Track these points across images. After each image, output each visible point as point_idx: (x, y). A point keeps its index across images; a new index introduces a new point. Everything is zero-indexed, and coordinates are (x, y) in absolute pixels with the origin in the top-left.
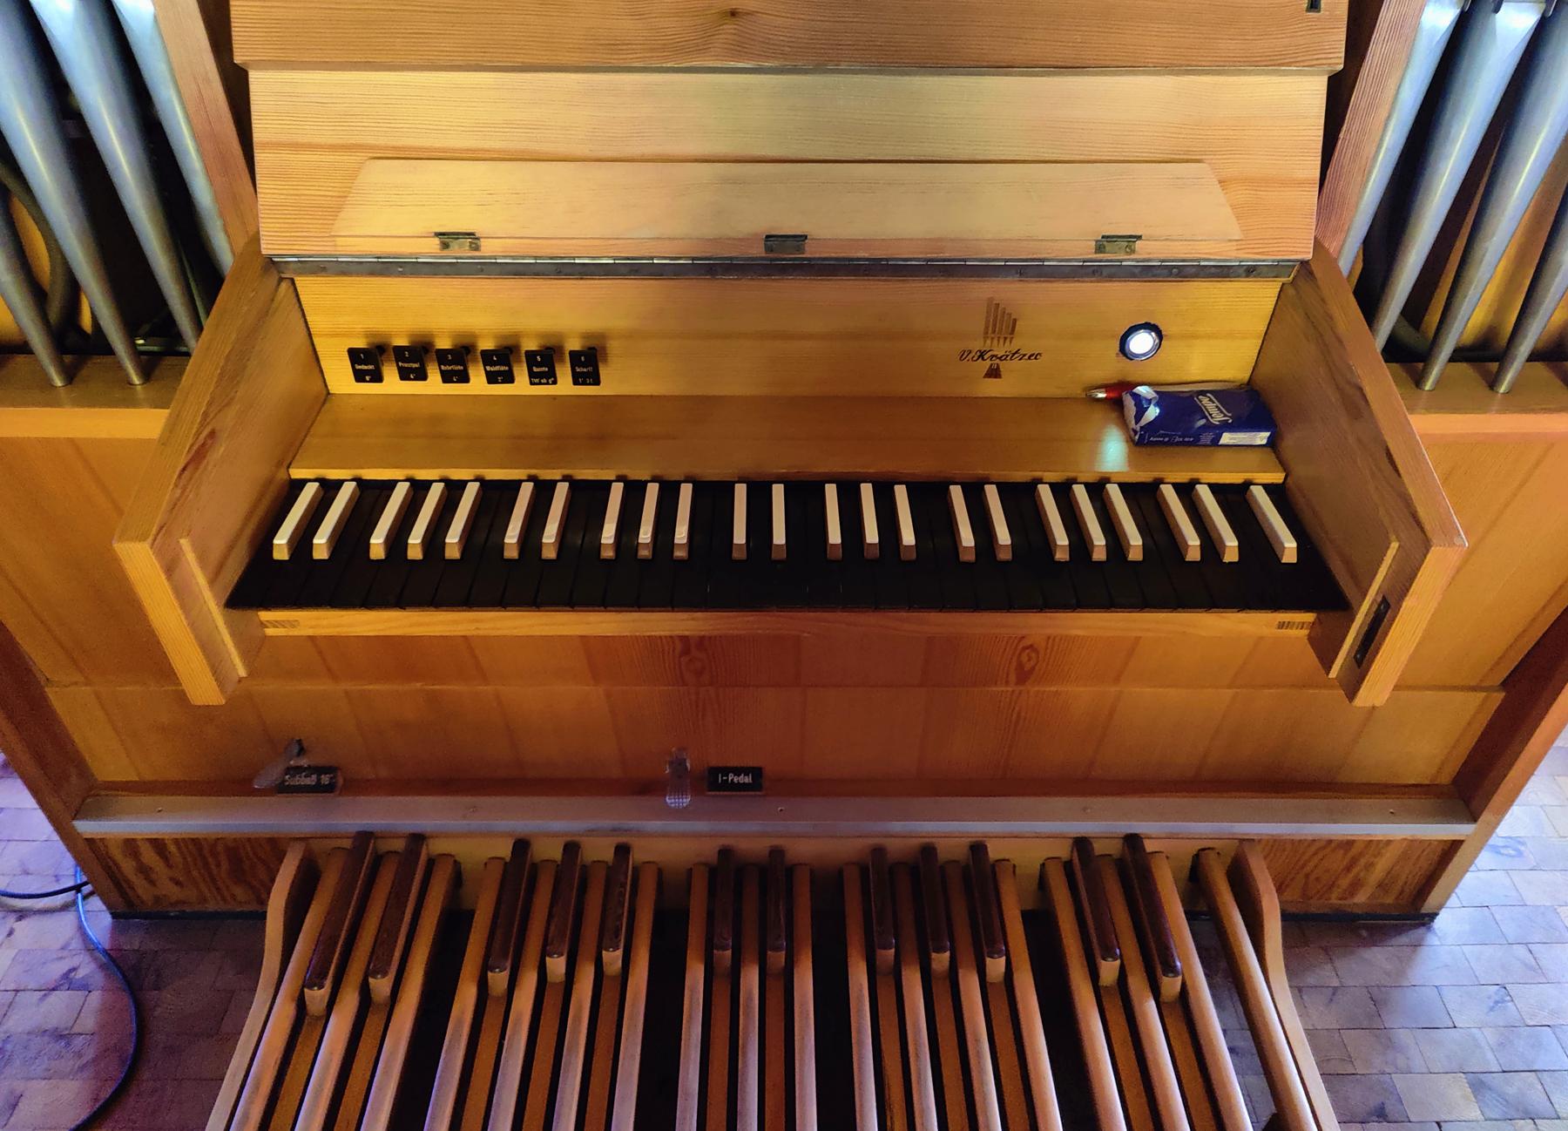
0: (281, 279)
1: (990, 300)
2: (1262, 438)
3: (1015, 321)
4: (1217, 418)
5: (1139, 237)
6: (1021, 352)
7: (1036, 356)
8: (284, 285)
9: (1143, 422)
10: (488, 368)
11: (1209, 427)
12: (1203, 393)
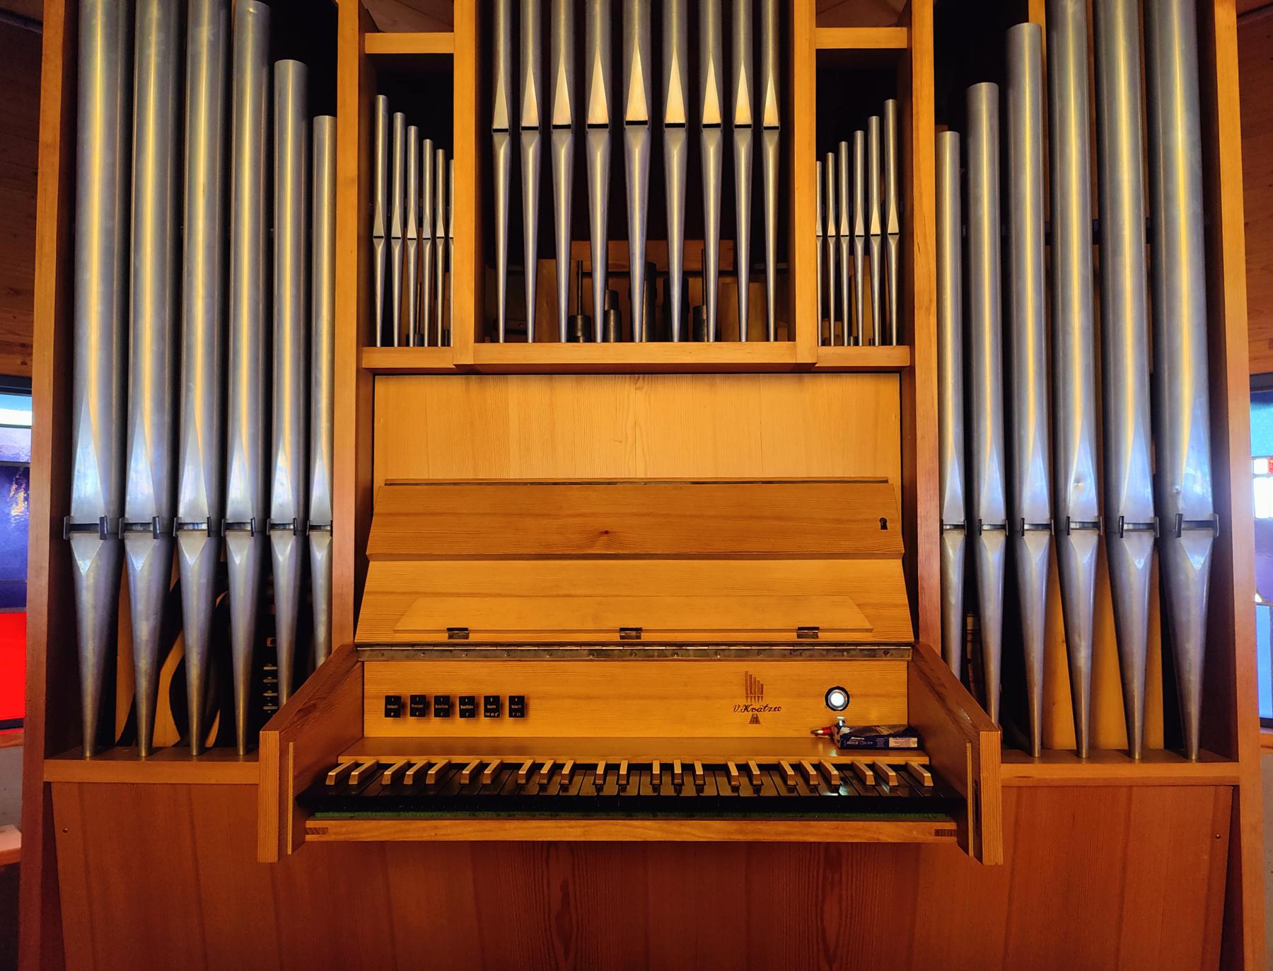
0: (358, 661)
1: (746, 672)
3: (762, 685)
5: (817, 629)
6: (769, 706)
7: (777, 709)
8: (359, 664)
10: (462, 707)
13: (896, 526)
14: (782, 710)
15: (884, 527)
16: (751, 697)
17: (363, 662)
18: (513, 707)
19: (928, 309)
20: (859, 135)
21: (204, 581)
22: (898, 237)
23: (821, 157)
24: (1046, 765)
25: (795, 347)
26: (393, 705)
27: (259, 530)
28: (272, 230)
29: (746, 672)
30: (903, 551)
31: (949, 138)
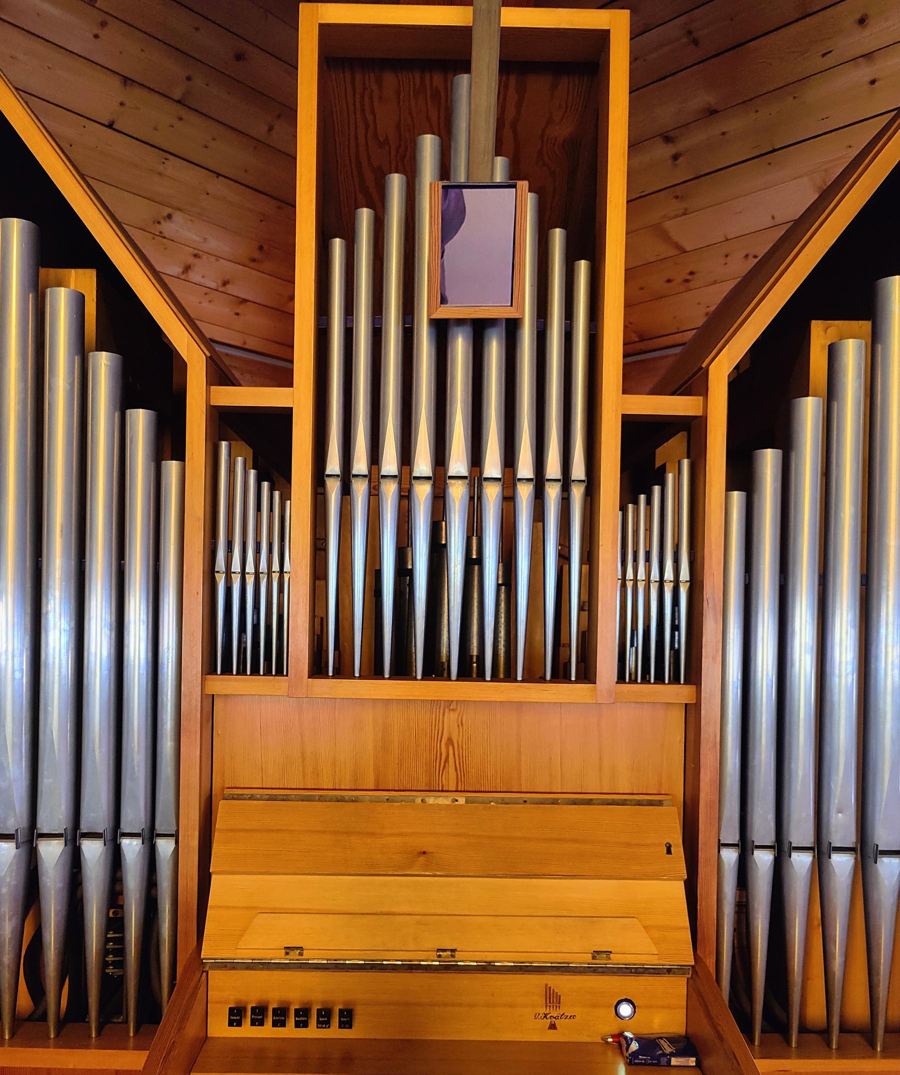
0: (203, 972)
2: (692, 1061)
4: (668, 1050)
5: (611, 952)
7: (574, 1017)
9: (630, 1051)
10: (297, 1019)
11: (664, 1055)
12: (661, 1038)
13: (679, 851)
14: (576, 1018)
15: (669, 852)
16: (550, 1006)
17: (207, 972)
18: (342, 1019)
19: (714, 658)
20: (657, 489)
21: (60, 885)
22: (688, 584)
23: (623, 509)
24: (802, 1061)
25: (595, 689)
26: (236, 1016)
27: (110, 839)
28: (122, 562)
29: (546, 985)
30: (686, 877)
31: (737, 497)
